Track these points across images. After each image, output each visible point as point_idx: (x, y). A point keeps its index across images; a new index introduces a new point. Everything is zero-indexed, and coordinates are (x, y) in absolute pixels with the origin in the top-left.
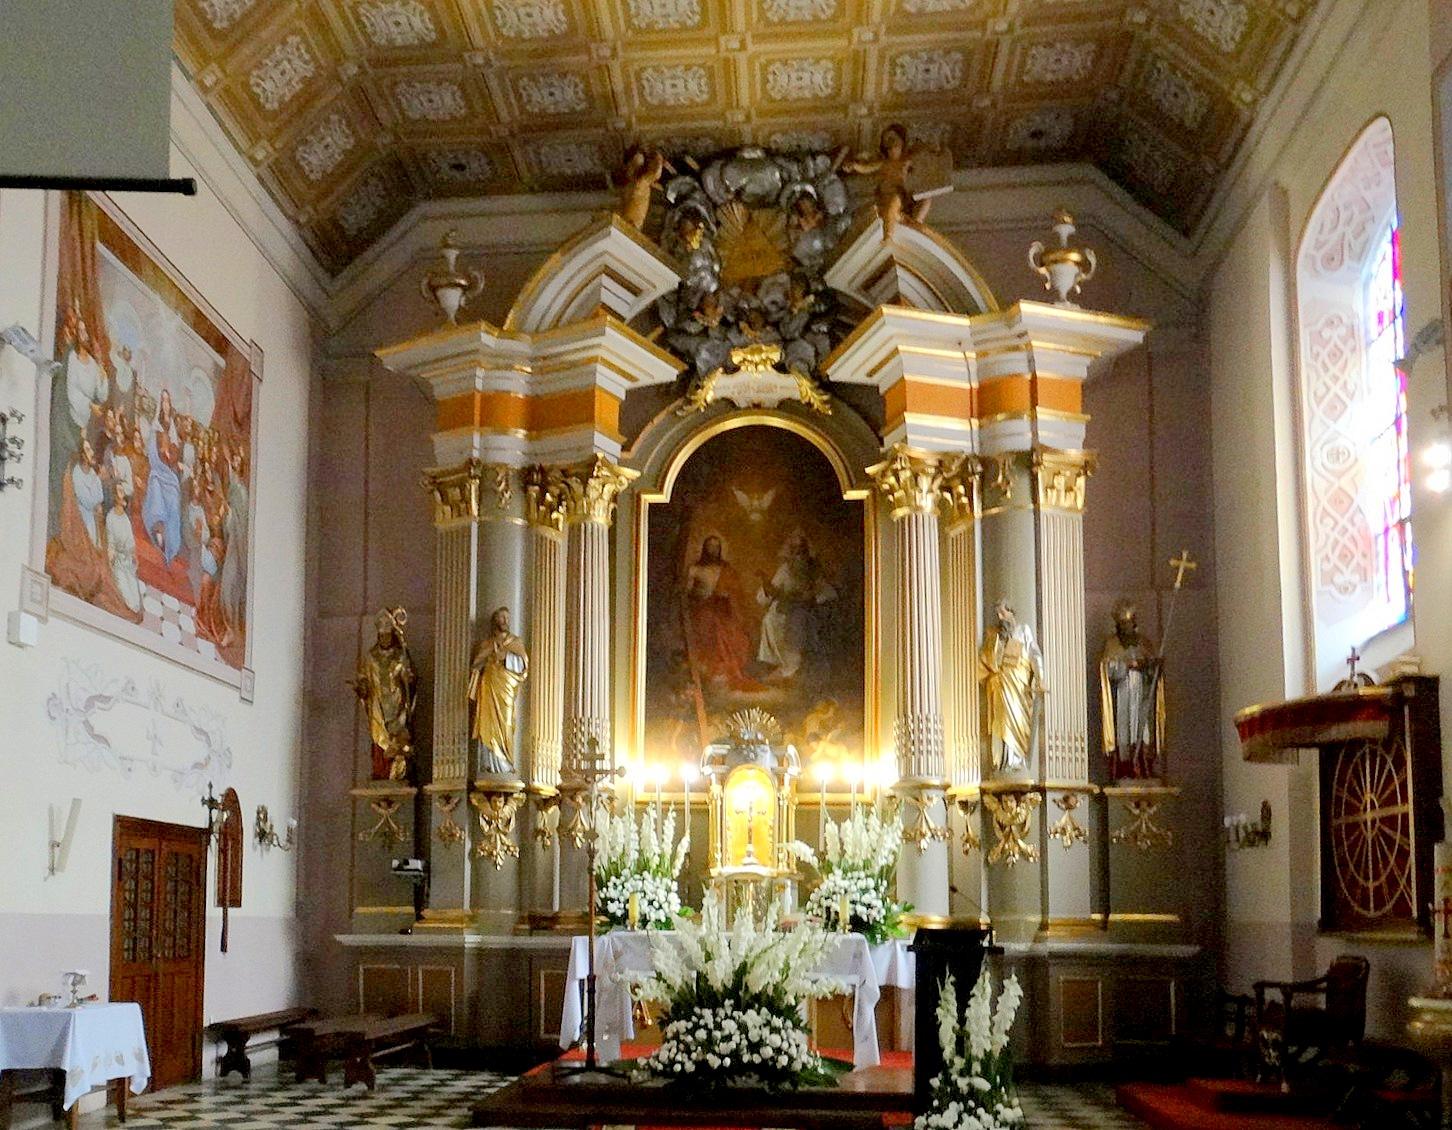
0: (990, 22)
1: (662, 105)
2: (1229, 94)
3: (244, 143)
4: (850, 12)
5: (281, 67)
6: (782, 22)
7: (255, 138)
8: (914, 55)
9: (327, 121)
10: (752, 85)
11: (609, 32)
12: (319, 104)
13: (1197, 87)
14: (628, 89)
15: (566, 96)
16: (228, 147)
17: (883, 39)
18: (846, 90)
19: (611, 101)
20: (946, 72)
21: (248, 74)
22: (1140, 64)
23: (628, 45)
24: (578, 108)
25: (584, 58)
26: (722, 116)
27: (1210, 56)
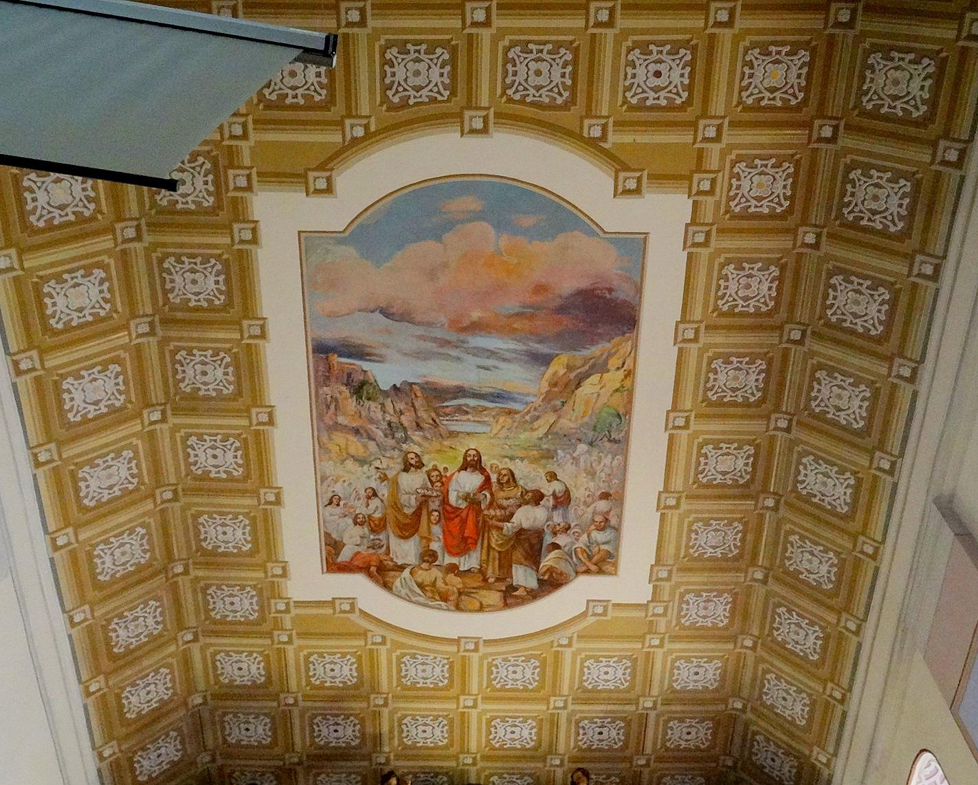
0: (642, 699)
1: (414, 747)
2: (810, 756)
3: (98, 742)
4: (548, 688)
5: (148, 689)
6: (503, 689)
7: (109, 737)
8: (591, 720)
9: (167, 735)
10: (479, 737)
11: (384, 686)
12: (164, 723)
13: (787, 754)
14: (391, 731)
15: (347, 734)
16: (87, 744)
17: (570, 707)
18: (545, 744)
19: (377, 740)
20: (613, 735)
21: (123, 689)
22: (744, 740)
23: (395, 697)
24: (353, 744)
25: (364, 705)
26: (456, 757)
27: (788, 726)
